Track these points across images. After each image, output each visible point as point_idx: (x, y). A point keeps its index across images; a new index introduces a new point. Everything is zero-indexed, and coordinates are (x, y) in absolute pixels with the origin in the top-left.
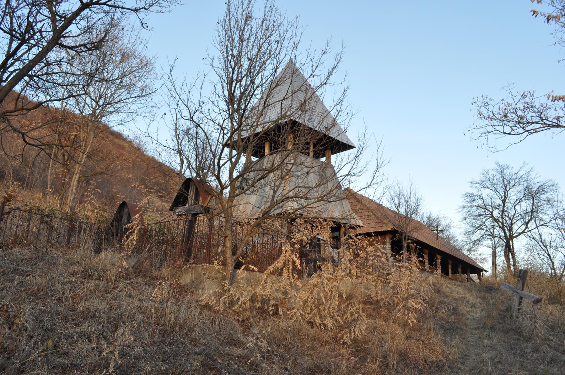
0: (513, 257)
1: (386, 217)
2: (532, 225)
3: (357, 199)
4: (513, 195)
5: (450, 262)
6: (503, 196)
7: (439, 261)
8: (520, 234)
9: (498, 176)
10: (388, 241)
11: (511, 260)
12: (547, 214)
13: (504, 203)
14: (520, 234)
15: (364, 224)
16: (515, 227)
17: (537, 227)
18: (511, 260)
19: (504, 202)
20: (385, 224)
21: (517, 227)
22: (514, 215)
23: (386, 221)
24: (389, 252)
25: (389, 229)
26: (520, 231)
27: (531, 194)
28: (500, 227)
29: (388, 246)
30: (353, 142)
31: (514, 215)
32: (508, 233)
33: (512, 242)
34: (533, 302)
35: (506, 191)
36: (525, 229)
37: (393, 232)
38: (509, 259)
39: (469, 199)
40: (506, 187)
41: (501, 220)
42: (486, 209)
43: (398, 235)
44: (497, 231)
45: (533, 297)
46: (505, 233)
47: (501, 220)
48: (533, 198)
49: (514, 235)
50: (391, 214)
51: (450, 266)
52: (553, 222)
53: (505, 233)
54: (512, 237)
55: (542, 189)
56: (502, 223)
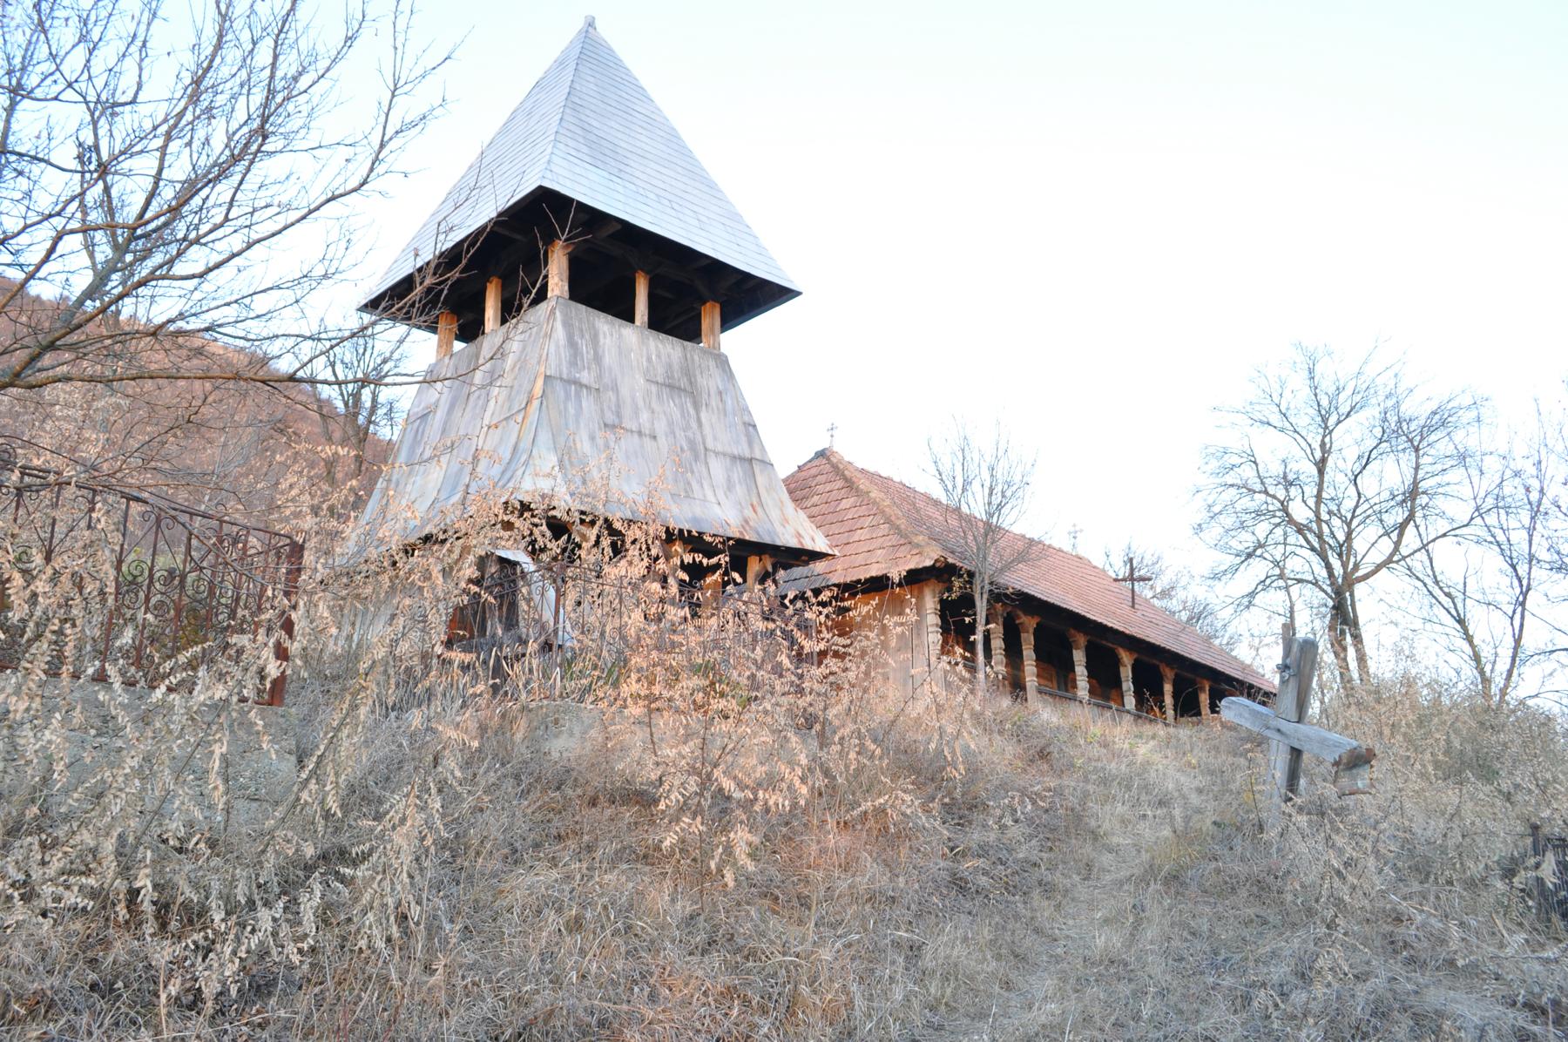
0: (1357, 638)
1: (919, 521)
2: (1411, 539)
3: (846, 479)
4: (1350, 439)
5: (1169, 674)
6: (1316, 446)
7: (1126, 673)
8: (1378, 568)
9: (1299, 382)
10: (931, 603)
11: (1351, 653)
12: (1453, 500)
13: (1321, 472)
14: (1378, 568)
15: (831, 547)
16: (1359, 545)
17: (1424, 546)
18: (1351, 653)
19: (1321, 466)
20: (918, 546)
21: (1370, 544)
22: (1357, 507)
23: (920, 539)
24: (934, 637)
25: (929, 563)
26: (1377, 556)
27: (1406, 435)
28: (1313, 549)
29: (933, 619)
30: (564, 44)
31: (1357, 507)
32: (1338, 570)
33: (1352, 595)
34: (1336, 764)
35: (1327, 431)
36: (1392, 554)
37: (941, 573)
38: (1345, 649)
39: (1214, 464)
40: (1325, 420)
41: (1314, 526)
42: (1266, 492)
43: (957, 583)
44: (1303, 562)
45: (1337, 745)
46: (1329, 567)
47: (1314, 526)
48: (1417, 450)
49: (1360, 573)
50: (931, 511)
51: (1168, 688)
52: (1478, 521)
53: (1329, 567)
54: (1350, 581)
55: (1440, 421)
56: (1320, 536)
